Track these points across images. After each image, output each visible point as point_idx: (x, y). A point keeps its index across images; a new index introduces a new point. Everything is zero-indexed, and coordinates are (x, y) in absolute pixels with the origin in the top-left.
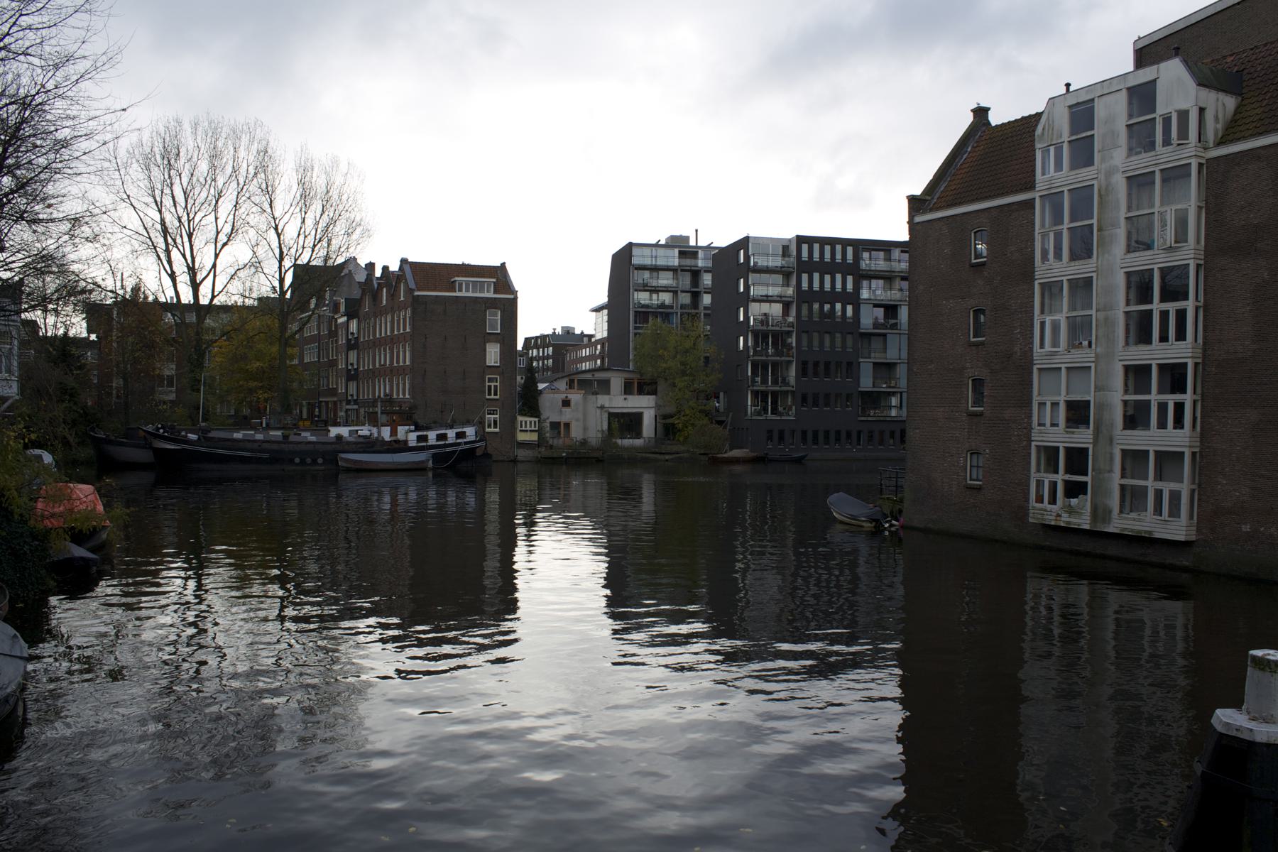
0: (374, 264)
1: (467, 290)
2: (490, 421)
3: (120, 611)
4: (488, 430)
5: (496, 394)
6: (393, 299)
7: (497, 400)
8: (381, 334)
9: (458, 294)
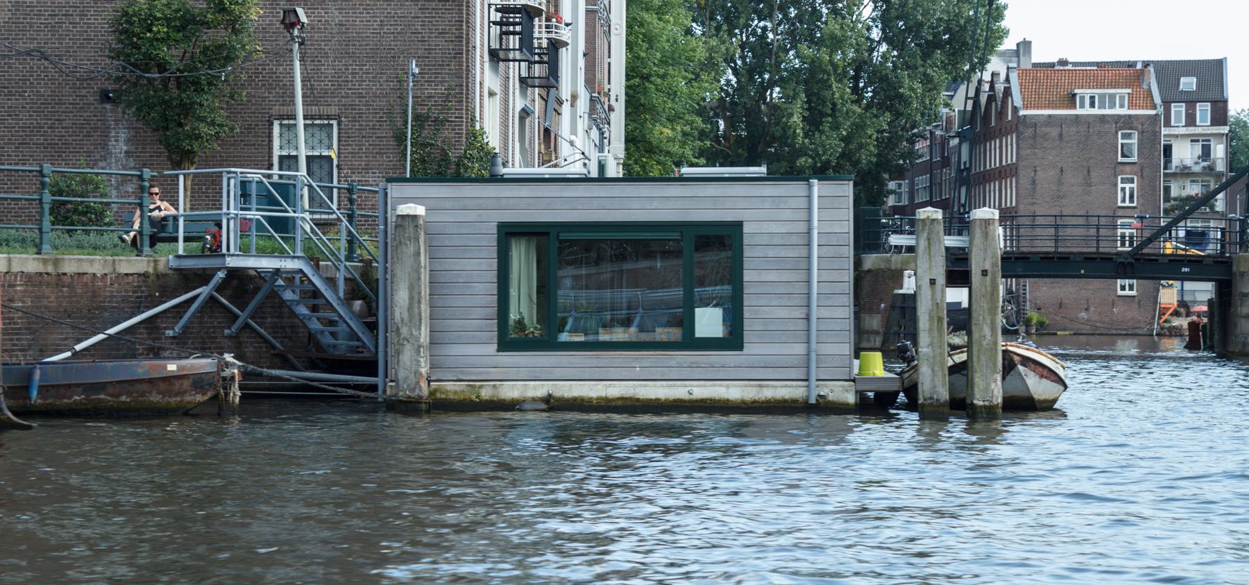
0: (1030, 43)
1: (1122, 106)
2: (1123, 236)
4: (1120, 292)
5: (1131, 199)
6: (1001, 119)
7: (1134, 208)
8: (990, 166)
9: (1078, 111)
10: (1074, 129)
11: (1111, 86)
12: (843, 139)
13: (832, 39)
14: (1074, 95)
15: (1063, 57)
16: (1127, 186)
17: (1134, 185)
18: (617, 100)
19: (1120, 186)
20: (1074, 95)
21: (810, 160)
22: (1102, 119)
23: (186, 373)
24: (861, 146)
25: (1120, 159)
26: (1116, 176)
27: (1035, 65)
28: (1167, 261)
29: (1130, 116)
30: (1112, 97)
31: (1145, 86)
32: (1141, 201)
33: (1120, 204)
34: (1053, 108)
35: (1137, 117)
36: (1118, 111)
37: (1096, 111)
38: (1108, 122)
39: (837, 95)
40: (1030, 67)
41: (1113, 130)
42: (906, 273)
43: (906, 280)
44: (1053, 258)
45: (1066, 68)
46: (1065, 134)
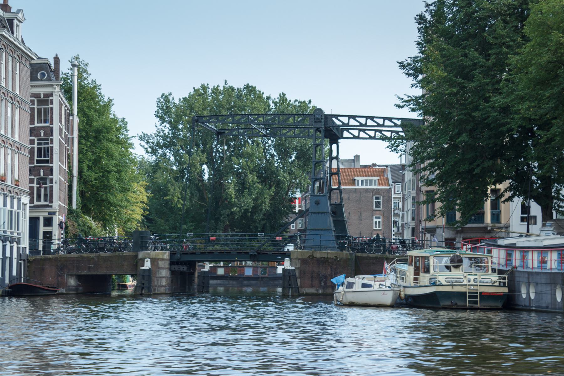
0: (359, 156)
1: (375, 185)
3: (230, 325)
5: (379, 227)
7: (381, 230)
9: (356, 187)
10: (355, 195)
11: (372, 176)
12: (254, 200)
13: (248, 154)
14: (355, 180)
15: (375, 162)
16: (378, 220)
17: (380, 220)
18: (56, 183)
19: (374, 220)
20: (355, 180)
21: (238, 209)
22: (367, 190)
23: (457, 289)
24: (262, 202)
25: (374, 208)
26: (372, 216)
27: (361, 166)
28: (271, 254)
29: (378, 189)
30: (371, 181)
31: (386, 176)
32: (383, 227)
33: (374, 228)
34: (345, 186)
35: (381, 189)
36: (373, 187)
37: (364, 187)
38: (369, 192)
39: (250, 180)
40: (359, 167)
41: (371, 195)
42: (146, 260)
43: (146, 263)
44: (224, 253)
45: (375, 167)
46: (350, 197)
